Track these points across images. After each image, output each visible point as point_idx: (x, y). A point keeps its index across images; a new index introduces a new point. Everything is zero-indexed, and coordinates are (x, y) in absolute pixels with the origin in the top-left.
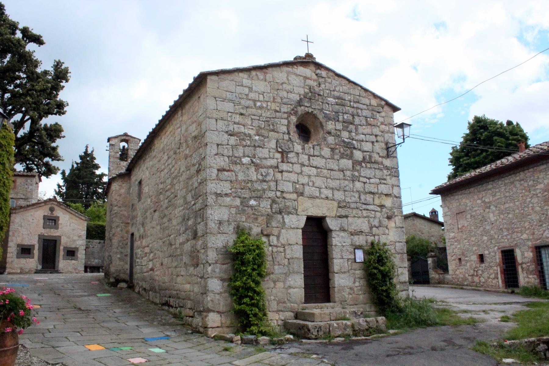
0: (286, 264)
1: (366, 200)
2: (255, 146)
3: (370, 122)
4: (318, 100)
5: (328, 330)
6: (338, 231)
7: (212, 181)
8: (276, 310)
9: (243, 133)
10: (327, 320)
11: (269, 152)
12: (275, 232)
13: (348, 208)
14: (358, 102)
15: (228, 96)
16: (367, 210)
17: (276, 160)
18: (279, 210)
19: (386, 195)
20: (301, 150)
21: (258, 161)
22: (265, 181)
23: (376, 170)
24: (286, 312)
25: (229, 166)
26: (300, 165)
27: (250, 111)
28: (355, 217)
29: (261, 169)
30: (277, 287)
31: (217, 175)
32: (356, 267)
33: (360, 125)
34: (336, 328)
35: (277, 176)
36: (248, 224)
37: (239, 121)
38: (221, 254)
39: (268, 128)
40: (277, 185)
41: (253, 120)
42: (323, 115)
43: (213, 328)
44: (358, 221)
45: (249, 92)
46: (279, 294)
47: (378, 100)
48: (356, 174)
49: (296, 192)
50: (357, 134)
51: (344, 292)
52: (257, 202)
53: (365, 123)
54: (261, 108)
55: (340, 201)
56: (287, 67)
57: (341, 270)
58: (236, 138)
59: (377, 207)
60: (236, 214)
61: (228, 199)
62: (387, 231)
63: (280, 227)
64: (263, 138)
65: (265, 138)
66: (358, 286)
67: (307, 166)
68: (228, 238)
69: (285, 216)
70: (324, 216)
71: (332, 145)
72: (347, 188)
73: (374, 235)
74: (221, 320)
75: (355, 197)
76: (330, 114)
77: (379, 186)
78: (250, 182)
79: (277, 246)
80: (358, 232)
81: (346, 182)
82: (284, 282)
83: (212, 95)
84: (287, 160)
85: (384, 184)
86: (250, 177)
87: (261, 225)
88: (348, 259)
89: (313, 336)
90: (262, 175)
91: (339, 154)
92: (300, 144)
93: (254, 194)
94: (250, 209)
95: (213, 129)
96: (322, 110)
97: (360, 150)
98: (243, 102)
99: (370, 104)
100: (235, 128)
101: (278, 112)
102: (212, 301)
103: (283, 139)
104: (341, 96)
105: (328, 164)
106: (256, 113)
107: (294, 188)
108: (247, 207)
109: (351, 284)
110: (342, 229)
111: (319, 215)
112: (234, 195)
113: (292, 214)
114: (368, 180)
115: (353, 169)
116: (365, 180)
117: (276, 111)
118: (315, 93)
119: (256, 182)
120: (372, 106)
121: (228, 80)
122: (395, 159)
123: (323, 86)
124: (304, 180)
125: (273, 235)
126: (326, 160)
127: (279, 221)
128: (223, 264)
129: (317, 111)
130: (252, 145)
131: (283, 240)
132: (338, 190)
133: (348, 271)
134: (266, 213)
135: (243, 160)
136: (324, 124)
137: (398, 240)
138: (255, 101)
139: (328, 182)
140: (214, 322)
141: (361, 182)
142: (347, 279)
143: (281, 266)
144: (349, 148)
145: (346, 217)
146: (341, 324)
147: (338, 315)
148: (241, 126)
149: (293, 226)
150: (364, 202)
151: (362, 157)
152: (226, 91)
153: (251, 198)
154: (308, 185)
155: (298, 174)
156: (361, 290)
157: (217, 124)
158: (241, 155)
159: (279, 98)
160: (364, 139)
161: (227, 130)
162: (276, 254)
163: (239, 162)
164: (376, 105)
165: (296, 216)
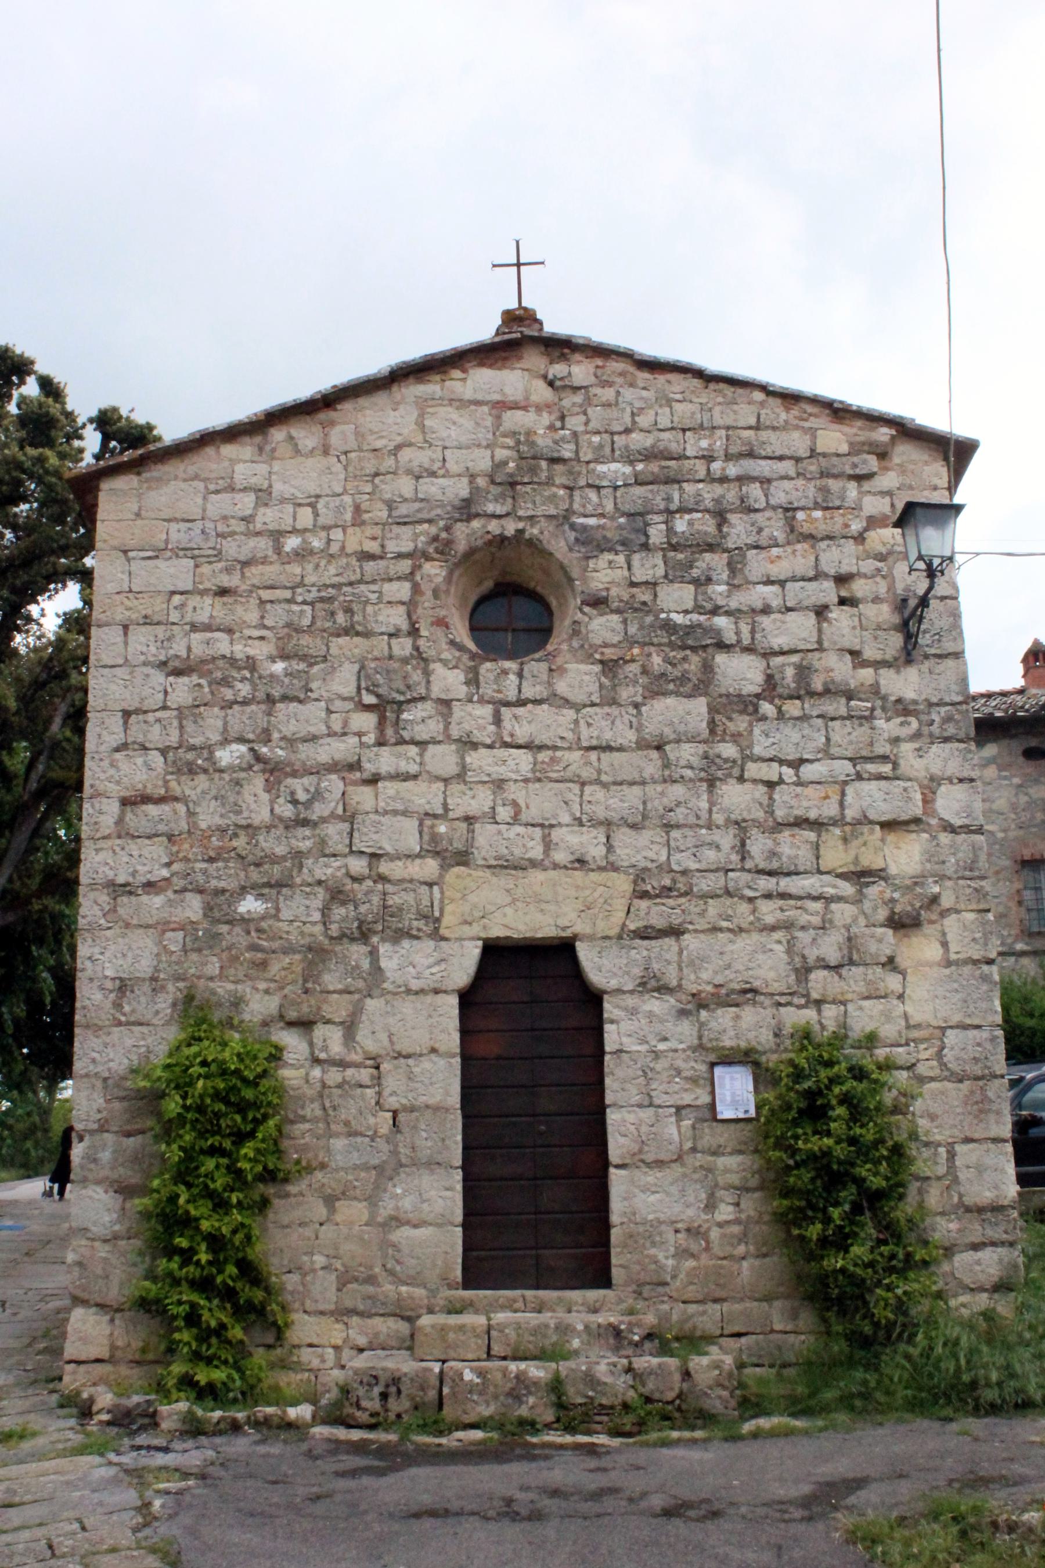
0: (385, 1129)
1: (773, 854)
2: (270, 700)
3: (806, 528)
4: (549, 482)
5: (432, 1394)
6: (632, 992)
7: (101, 844)
8: (332, 1307)
9: (224, 657)
10: (470, 1356)
11: (329, 712)
12: (338, 1008)
13: (681, 895)
14: (751, 455)
15: (174, 536)
16: (784, 896)
17: (354, 740)
18: (359, 927)
19: (889, 825)
20: (465, 688)
21: (280, 752)
22: (305, 823)
23: (837, 724)
24: (378, 1320)
25: (166, 782)
26: (453, 747)
27: (256, 574)
28: (715, 929)
29: (289, 781)
30: (338, 1218)
31: (120, 821)
32: (722, 1141)
33: (757, 547)
34: (471, 1388)
35: (356, 798)
36: (231, 987)
37: (211, 617)
38: (122, 1099)
39: (328, 624)
40: (351, 834)
41: (268, 606)
42: (572, 536)
43: (79, 1363)
44: (731, 947)
45: (257, 506)
46: (346, 1248)
47: (855, 430)
48: (728, 750)
49: (434, 848)
50: (733, 587)
51: (654, 1244)
52: (267, 901)
53: (780, 535)
54: (302, 555)
55: (646, 869)
56: (420, 381)
57: (640, 1151)
58: (195, 679)
59: (840, 882)
60: (185, 951)
61: (158, 900)
62: (893, 982)
63: (358, 991)
64: (302, 666)
65: (311, 665)
66: (728, 1222)
67: (490, 747)
68: (150, 1040)
69: (384, 949)
70: (568, 933)
71: (606, 651)
72: (679, 815)
73: (818, 1003)
74: (111, 1334)
75: (718, 847)
76: (602, 527)
77: (849, 790)
78: (242, 833)
79: (342, 1064)
80: (733, 991)
81: (678, 791)
82: (372, 1200)
83: (115, 543)
84: (397, 732)
85: (880, 777)
86: (245, 814)
87: (282, 988)
88: (679, 1109)
89: (358, 1414)
90: (295, 802)
91: (643, 680)
92: (455, 667)
93: (255, 875)
94: (238, 930)
95: (110, 663)
96: (566, 518)
97: (749, 650)
98: (231, 548)
99: (812, 450)
100: (194, 645)
101: (370, 557)
102: (80, 1264)
103: (391, 657)
104: (661, 445)
105: (589, 725)
106: (283, 580)
107: (426, 838)
108: (227, 922)
109: (692, 1213)
110: (653, 983)
111: (539, 935)
112: (178, 883)
113: (417, 938)
114: (788, 772)
115: (712, 731)
116: (772, 772)
117: (366, 556)
118: (534, 458)
119: (269, 828)
120: (824, 455)
121: (176, 478)
122: (950, 663)
123: (575, 422)
124: (479, 801)
125: (328, 1022)
126: (578, 711)
127: (357, 967)
128: (128, 1135)
129: (543, 522)
130: (260, 695)
131: (368, 1040)
132: (634, 826)
133: (679, 1159)
134: (306, 941)
135: (218, 754)
136: (575, 573)
137: (956, 1018)
138: (277, 536)
139: (586, 798)
140: (84, 1340)
141: (755, 781)
142: (674, 1190)
143: (359, 1139)
144: (693, 649)
145: (675, 932)
146: (499, 1376)
147: (527, 1337)
148: (218, 635)
149: (415, 985)
150: (762, 865)
151: (760, 678)
152: (169, 521)
153: (243, 890)
154: (492, 817)
155: (446, 781)
156: (743, 1238)
157: (126, 643)
158: (215, 737)
159: (380, 505)
160: (775, 603)
161: (163, 658)
162: (337, 1092)
163: (206, 765)
164: (844, 448)
165: (432, 943)
